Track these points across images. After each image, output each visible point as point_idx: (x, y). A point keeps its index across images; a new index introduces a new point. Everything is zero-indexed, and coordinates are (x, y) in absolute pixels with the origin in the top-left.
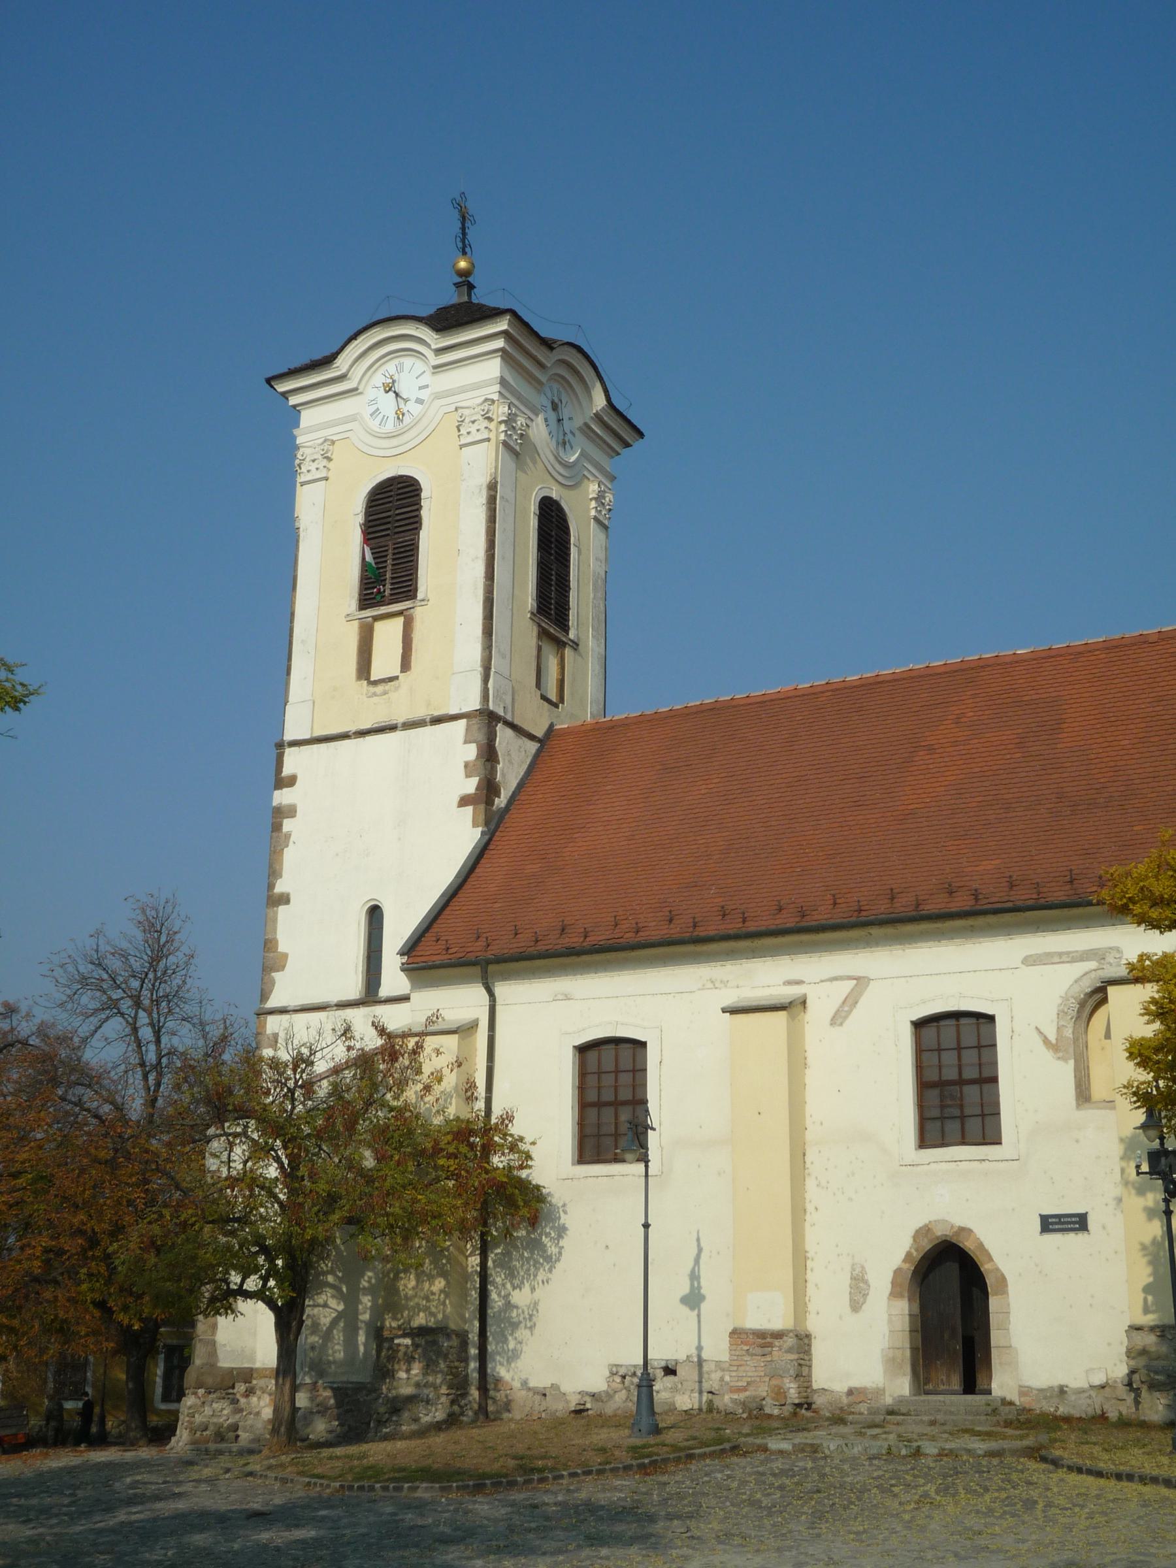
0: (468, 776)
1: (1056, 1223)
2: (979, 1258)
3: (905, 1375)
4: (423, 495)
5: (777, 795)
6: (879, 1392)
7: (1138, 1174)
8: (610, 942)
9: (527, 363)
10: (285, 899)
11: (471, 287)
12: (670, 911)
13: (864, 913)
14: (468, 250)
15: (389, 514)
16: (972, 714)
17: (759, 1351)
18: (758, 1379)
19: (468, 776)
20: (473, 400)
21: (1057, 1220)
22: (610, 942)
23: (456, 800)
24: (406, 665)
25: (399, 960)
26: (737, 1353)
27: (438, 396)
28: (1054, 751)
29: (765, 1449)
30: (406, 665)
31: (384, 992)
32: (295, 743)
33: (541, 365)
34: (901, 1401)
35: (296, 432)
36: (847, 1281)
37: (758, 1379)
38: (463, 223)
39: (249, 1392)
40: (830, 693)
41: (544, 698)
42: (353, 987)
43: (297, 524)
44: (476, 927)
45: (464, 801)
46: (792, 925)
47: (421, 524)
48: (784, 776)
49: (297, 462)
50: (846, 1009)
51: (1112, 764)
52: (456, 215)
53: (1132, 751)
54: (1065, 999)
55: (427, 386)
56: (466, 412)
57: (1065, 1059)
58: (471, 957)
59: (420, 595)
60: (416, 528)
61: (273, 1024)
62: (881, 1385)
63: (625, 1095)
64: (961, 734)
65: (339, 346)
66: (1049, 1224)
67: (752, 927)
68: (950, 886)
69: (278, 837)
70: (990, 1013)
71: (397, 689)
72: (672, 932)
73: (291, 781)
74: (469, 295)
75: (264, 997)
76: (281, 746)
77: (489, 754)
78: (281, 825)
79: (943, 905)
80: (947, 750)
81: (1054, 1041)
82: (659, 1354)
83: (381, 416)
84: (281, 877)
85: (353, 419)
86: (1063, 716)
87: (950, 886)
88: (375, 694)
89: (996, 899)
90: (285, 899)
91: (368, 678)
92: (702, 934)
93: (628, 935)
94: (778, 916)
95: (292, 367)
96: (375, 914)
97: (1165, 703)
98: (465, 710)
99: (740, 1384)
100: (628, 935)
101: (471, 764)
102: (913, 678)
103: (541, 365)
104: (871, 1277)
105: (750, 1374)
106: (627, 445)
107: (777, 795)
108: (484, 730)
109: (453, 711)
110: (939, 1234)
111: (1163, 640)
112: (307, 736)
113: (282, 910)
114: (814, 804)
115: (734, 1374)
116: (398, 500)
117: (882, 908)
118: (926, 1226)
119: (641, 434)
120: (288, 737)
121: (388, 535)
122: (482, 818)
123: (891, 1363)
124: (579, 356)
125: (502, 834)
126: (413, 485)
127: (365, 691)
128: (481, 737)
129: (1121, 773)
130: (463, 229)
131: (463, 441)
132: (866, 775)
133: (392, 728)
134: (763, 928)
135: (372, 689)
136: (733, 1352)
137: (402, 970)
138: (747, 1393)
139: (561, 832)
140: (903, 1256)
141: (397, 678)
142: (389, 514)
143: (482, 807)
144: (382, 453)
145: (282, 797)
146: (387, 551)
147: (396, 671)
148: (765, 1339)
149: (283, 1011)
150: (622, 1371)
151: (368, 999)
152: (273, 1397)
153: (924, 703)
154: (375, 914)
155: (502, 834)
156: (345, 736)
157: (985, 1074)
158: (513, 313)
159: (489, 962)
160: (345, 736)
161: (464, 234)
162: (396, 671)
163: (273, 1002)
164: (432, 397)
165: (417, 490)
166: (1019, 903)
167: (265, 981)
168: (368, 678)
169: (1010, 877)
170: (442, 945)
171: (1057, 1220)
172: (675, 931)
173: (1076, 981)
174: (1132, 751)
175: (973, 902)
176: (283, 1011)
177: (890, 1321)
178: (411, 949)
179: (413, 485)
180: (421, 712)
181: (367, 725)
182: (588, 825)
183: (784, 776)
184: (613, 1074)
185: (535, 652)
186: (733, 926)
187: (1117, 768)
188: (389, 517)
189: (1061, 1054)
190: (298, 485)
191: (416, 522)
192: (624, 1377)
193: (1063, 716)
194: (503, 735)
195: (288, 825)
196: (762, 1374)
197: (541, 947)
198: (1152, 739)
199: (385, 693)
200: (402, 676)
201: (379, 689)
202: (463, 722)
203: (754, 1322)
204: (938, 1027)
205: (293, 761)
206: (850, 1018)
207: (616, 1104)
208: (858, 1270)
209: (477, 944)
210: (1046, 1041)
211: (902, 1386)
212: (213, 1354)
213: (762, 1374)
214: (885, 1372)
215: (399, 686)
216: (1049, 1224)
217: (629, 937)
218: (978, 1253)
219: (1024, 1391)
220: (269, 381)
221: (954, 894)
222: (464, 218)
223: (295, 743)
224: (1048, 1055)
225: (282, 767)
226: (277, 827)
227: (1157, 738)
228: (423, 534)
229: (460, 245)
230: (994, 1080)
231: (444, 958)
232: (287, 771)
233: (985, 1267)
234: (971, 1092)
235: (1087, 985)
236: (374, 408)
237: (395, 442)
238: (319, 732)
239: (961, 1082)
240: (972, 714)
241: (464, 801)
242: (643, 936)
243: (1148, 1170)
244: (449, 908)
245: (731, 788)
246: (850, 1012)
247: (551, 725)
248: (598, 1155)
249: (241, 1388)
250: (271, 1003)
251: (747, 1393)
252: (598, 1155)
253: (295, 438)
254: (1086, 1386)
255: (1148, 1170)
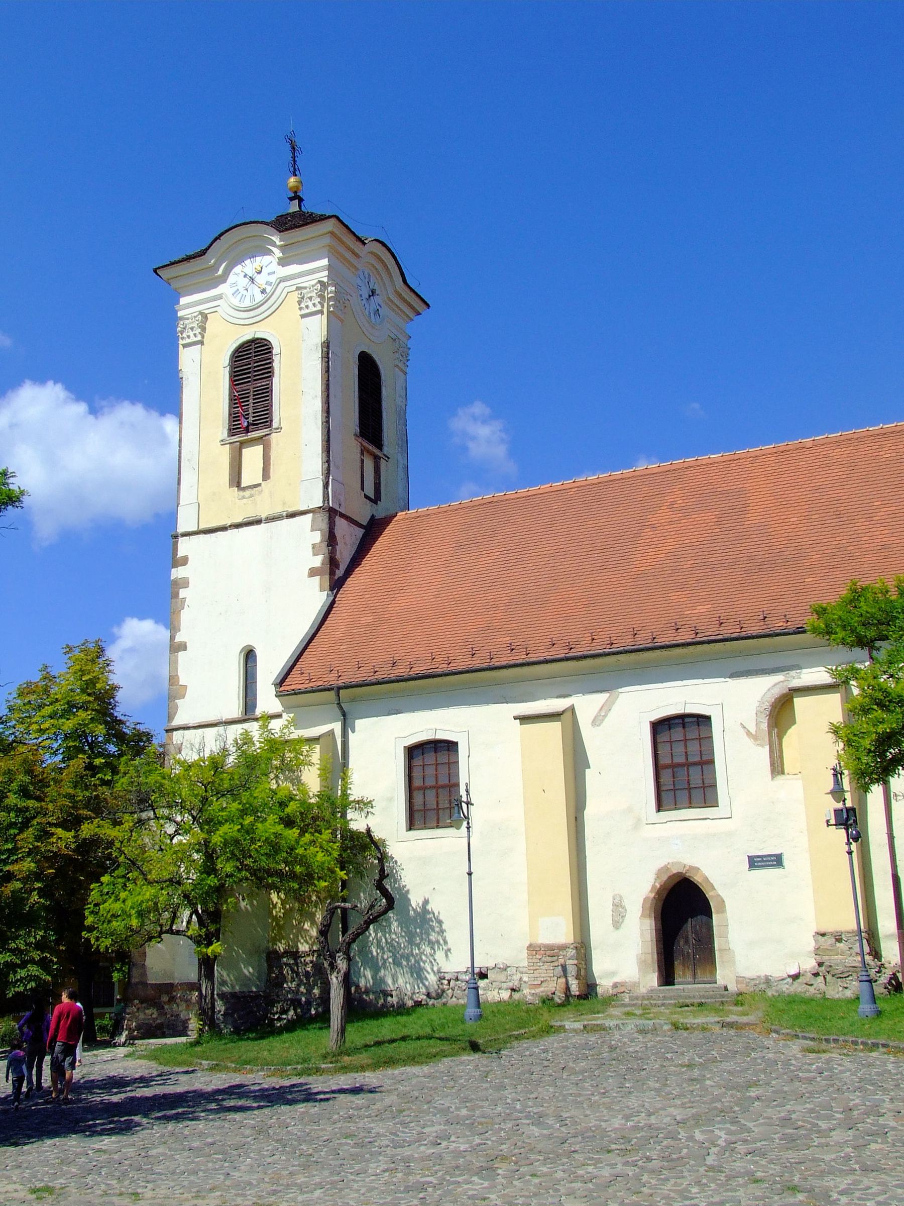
0: (315, 554)
1: (760, 861)
2: (704, 888)
3: (654, 972)
4: (274, 352)
5: (543, 563)
6: (636, 985)
7: (828, 825)
8: (429, 671)
9: (348, 255)
10: (183, 647)
11: (301, 200)
12: (472, 648)
13: (614, 646)
14: (297, 173)
15: (249, 366)
16: (681, 501)
17: (550, 959)
18: (549, 979)
19: (315, 554)
20: (310, 281)
21: (760, 859)
22: (429, 671)
23: (306, 572)
24: (266, 475)
25: (272, 690)
26: (533, 961)
27: (283, 280)
28: (742, 527)
29: (562, 1027)
30: (266, 475)
31: (258, 712)
32: (186, 534)
33: (357, 256)
34: (652, 990)
35: (177, 307)
36: (610, 907)
37: (549, 979)
38: (294, 153)
39: (172, 999)
40: (576, 489)
41: (366, 497)
42: (235, 710)
43: (181, 375)
44: (329, 663)
45: (313, 572)
46: (563, 655)
47: (273, 373)
48: (547, 549)
49: (179, 329)
50: (603, 714)
51: (786, 535)
52: (288, 147)
53: (800, 526)
54: (761, 702)
55: (274, 273)
56: (304, 291)
57: (762, 746)
58: (327, 685)
59: (275, 425)
60: (270, 377)
61: (177, 736)
62: (636, 980)
63: (443, 781)
64: (674, 516)
65: (208, 245)
66: (755, 862)
67: (533, 658)
68: (676, 624)
69: (176, 602)
70: (707, 714)
71: (261, 492)
72: (474, 662)
73: (184, 561)
74: (300, 207)
75: (170, 718)
76: (176, 537)
77: (331, 539)
78: (178, 594)
79: (672, 639)
80: (665, 527)
81: (754, 733)
82: (481, 962)
83: (240, 295)
84: (180, 631)
85: (220, 297)
86: (748, 502)
87: (676, 624)
88: (244, 497)
89: (711, 633)
90: (183, 647)
91: (238, 485)
92: (497, 664)
93: (441, 666)
94: (551, 650)
95: (172, 261)
96: (249, 655)
97: (822, 490)
98: (311, 507)
99: (536, 983)
100: (441, 666)
101: (318, 545)
102: (636, 477)
103: (357, 256)
104: (626, 903)
105: (543, 975)
106: (419, 314)
107: (543, 563)
108: (326, 520)
109: (304, 508)
110: (675, 872)
111: (816, 446)
112: (195, 529)
113: (181, 655)
114: (571, 569)
115: (532, 975)
116: (255, 356)
117: (627, 642)
118: (666, 866)
119: (428, 306)
120: (181, 529)
121: (249, 382)
122: (327, 584)
123: (642, 963)
124: (384, 249)
125: (342, 596)
126: (266, 345)
127: (236, 496)
128: (325, 526)
129: (793, 541)
130: (294, 157)
131: (303, 312)
132: (607, 547)
133: (258, 522)
134: (542, 658)
135: (241, 493)
136: (530, 961)
137: (276, 696)
138: (542, 989)
139: (386, 593)
140: (650, 889)
141: (259, 485)
142: (249, 366)
143: (327, 577)
144: (242, 322)
145: (178, 573)
146: (249, 393)
147: (259, 480)
148: (552, 951)
149: (186, 728)
150: (448, 977)
151: (247, 717)
152: (458, 998)
153: (645, 495)
154: (249, 655)
155: (342, 596)
156: (224, 529)
157: (705, 758)
158: (338, 218)
159: (339, 688)
160: (224, 529)
161: (295, 161)
162: (260, 481)
163: (177, 722)
164: (278, 281)
165: (270, 348)
166: (726, 636)
167: (171, 706)
168: (238, 485)
169: (720, 617)
170: (306, 677)
171: (760, 859)
172: (477, 663)
173: (769, 690)
174: (800, 526)
175: (694, 636)
176: (186, 728)
177: (642, 934)
178: (281, 682)
179: (266, 345)
180: (278, 509)
181: (239, 520)
182: (405, 588)
183: (547, 549)
184: (683, 743)
185: (359, 464)
186: (521, 658)
187: (790, 538)
188: (249, 368)
189: (759, 742)
190: (181, 347)
191: (270, 372)
192: (449, 981)
193: (748, 502)
194: (340, 523)
195: (182, 593)
196: (552, 975)
197: (378, 676)
198: (813, 517)
199: (251, 496)
200: (263, 483)
201: (247, 493)
202: (310, 516)
203: (830, 927)
204: (423, 749)
205: (185, 547)
206: (606, 720)
207: (688, 765)
208: (618, 899)
209: (330, 676)
210: (748, 733)
211: (653, 979)
212: (144, 974)
213: (552, 975)
214: (640, 970)
215: (262, 491)
216: (755, 862)
217: (444, 668)
218: (704, 884)
219: (739, 979)
220: (155, 271)
221: (679, 631)
222: (294, 148)
223: (186, 534)
224: (749, 742)
225: (177, 551)
226: (176, 595)
227: (817, 516)
228: (275, 380)
229: (292, 169)
230: (711, 762)
231: (309, 686)
232: (180, 554)
233: (709, 895)
234: (695, 772)
235: (777, 692)
236: (235, 289)
237: (252, 314)
238: (203, 526)
239: (688, 765)
240: (681, 501)
241: (313, 572)
242: (453, 667)
243: (834, 823)
244: (307, 650)
245: (508, 558)
246: (605, 716)
247: (373, 516)
248: (705, 803)
249: (165, 998)
250: (176, 722)
251: (542, 989)
252: (705, 803)
253: (176, 312)
254: (785, 976)
255: (834, 823)
